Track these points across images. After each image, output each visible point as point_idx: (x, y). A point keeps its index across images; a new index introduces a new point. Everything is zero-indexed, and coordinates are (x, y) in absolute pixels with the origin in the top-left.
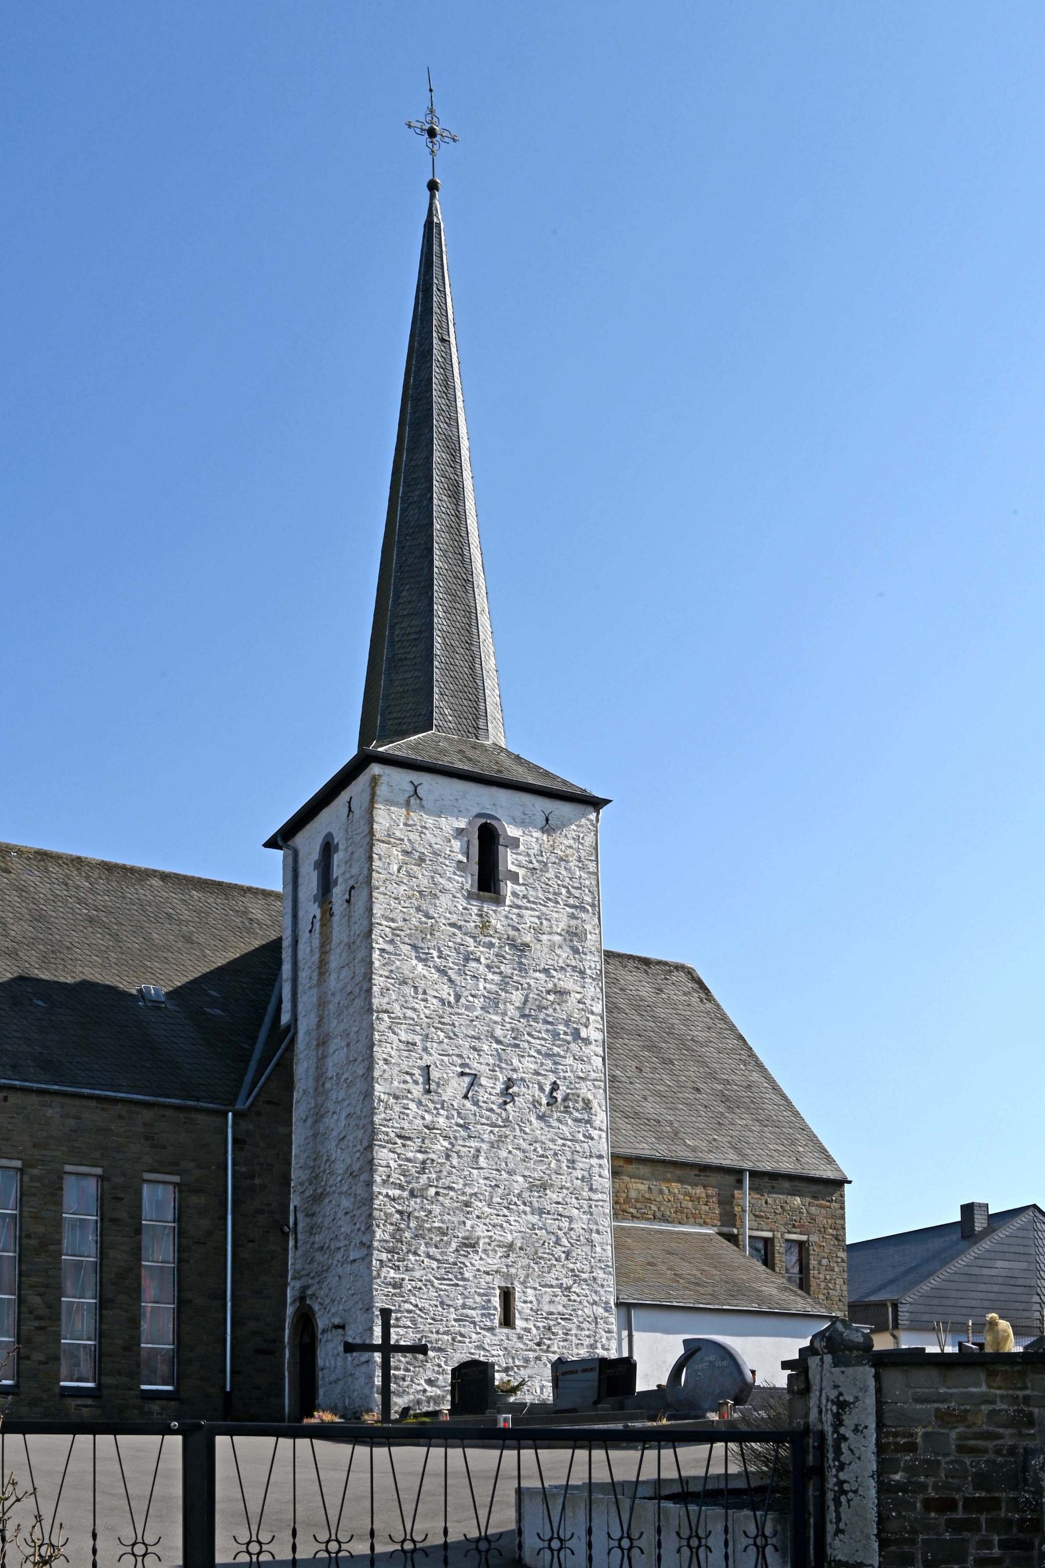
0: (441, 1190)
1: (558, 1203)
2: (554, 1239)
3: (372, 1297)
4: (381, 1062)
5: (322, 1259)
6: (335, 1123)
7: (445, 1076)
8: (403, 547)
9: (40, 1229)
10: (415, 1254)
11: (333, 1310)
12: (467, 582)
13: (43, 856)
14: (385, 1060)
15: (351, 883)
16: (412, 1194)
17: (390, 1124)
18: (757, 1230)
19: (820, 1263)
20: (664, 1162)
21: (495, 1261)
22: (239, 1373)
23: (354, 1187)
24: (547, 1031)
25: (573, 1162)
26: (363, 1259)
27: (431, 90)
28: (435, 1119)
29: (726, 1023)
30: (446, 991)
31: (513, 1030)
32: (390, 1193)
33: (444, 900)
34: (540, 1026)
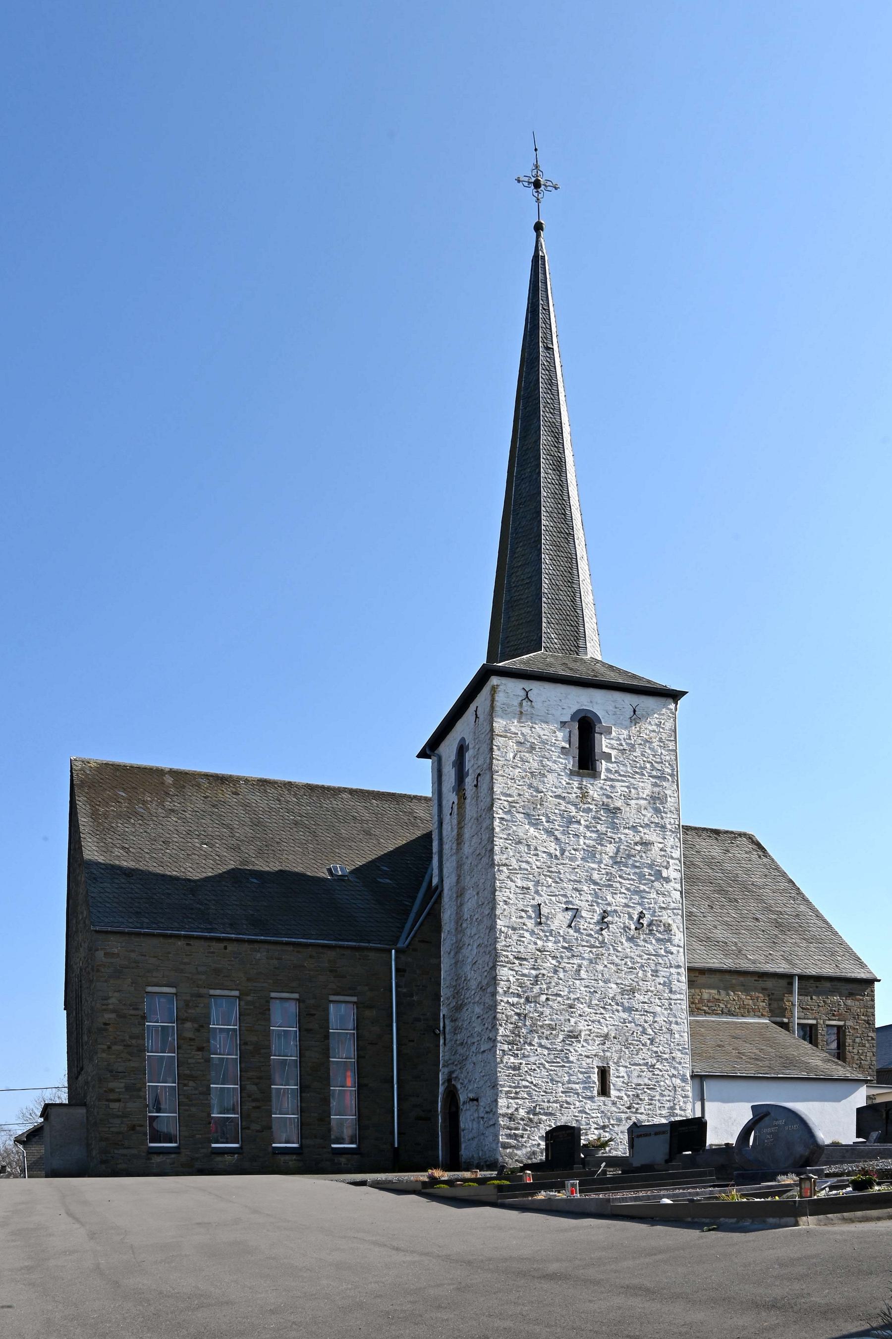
1: (645, 1003)
2: (641, 1029)
4: (501, 903)
5: (462, 1052)
6: (470, 953)
9: (254, 1039)
10: (530, 1044)
12: (569, 536)
13: (264, 782)
14: (505, 901)
15: (478, 771)
16: (528, 1000)
18: (804, 1019)
19: (854, 1041)
21: (594, 1048)
24: (635, 873)
25: (657, 971)
28: (545, 944)
30: (553, 847)
32: (510, 1000)
33: (551, 778)
34: (628, 870)
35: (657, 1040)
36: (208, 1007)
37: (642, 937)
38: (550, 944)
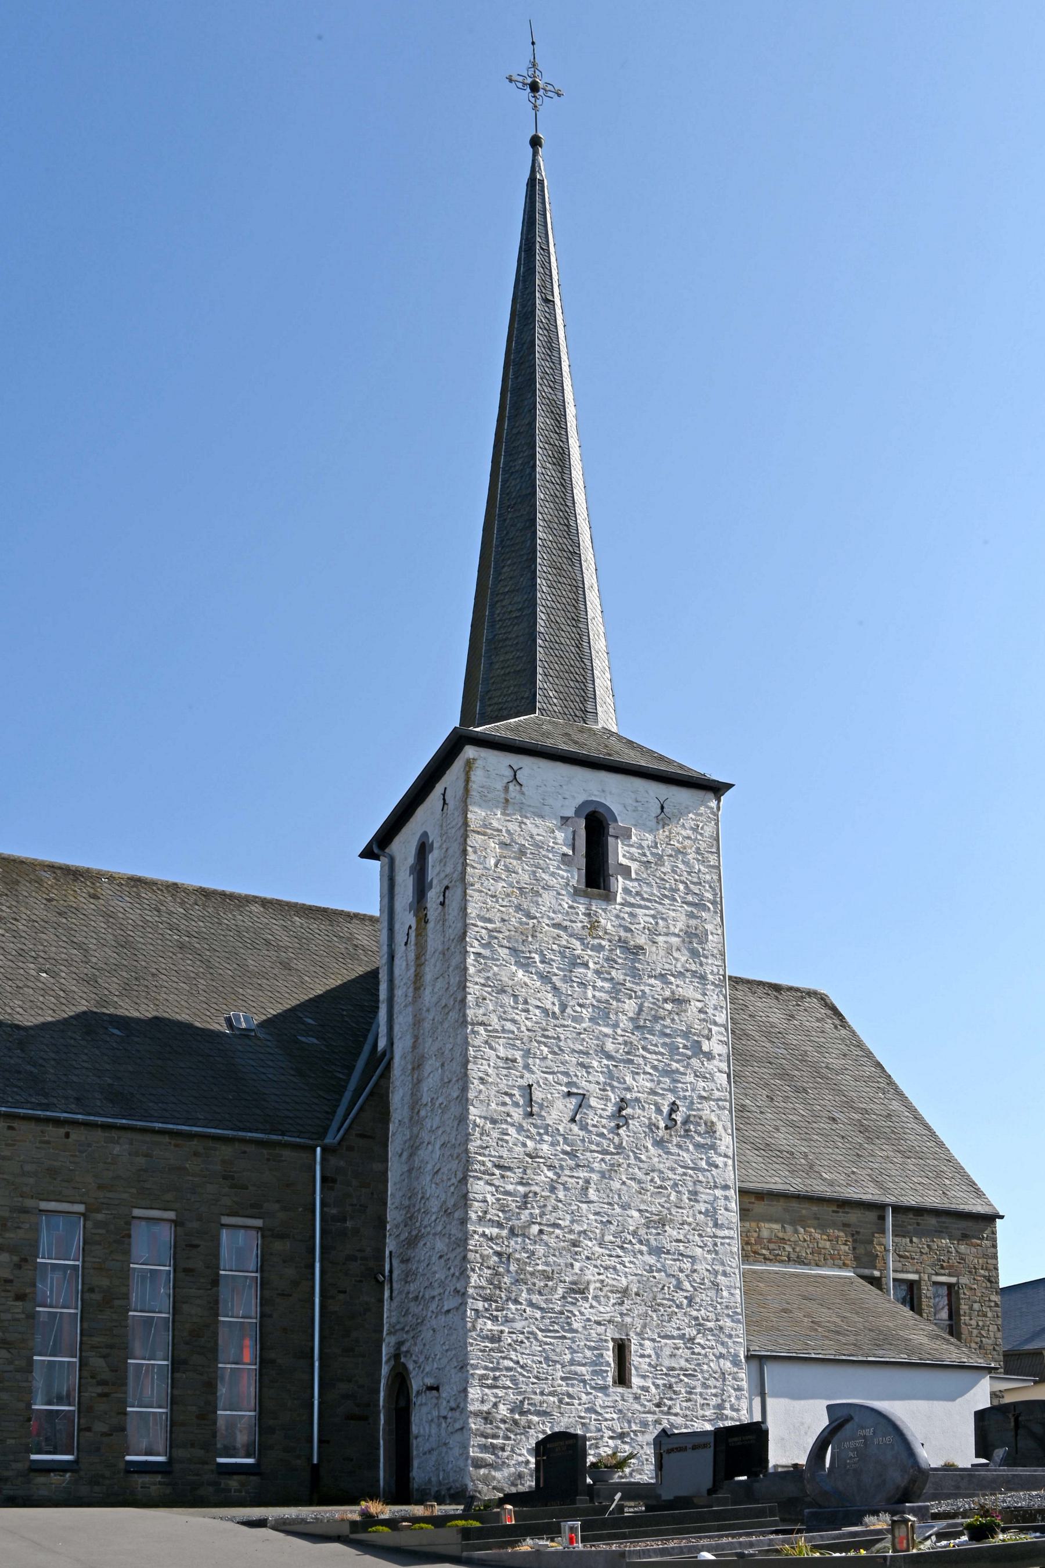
0: (545, 1228)
3: (466, 1354)
4: (476, 1082)
6: (431, 1155)
7: (549, 1096)
8: (505, 520)
9: (105, 1282)
10: (516, 1302)
11: (427, 1369)
12: (574, 555)
14: (481, 1079)
15: (446, 883)
16: (512, 1232)
17: (487, 1152)
18: (902, 1271)
19: (971, 1308)
20: (798, 1197)
21: (607, 1310)
22: (328, 1442)
23: (448, 1227)
25: (696, 1193)
26: (457, 1309)
27: (533, 43)
28: (538, 1146)
29: (862, 1050)
30: (549, 1000)
31: (626, 1043)
32: (487, 1231)
33: (547, 898)
35: (698, 1300)
36: (36, 1229)
37: (675, 1140)
38: (545, 1147)
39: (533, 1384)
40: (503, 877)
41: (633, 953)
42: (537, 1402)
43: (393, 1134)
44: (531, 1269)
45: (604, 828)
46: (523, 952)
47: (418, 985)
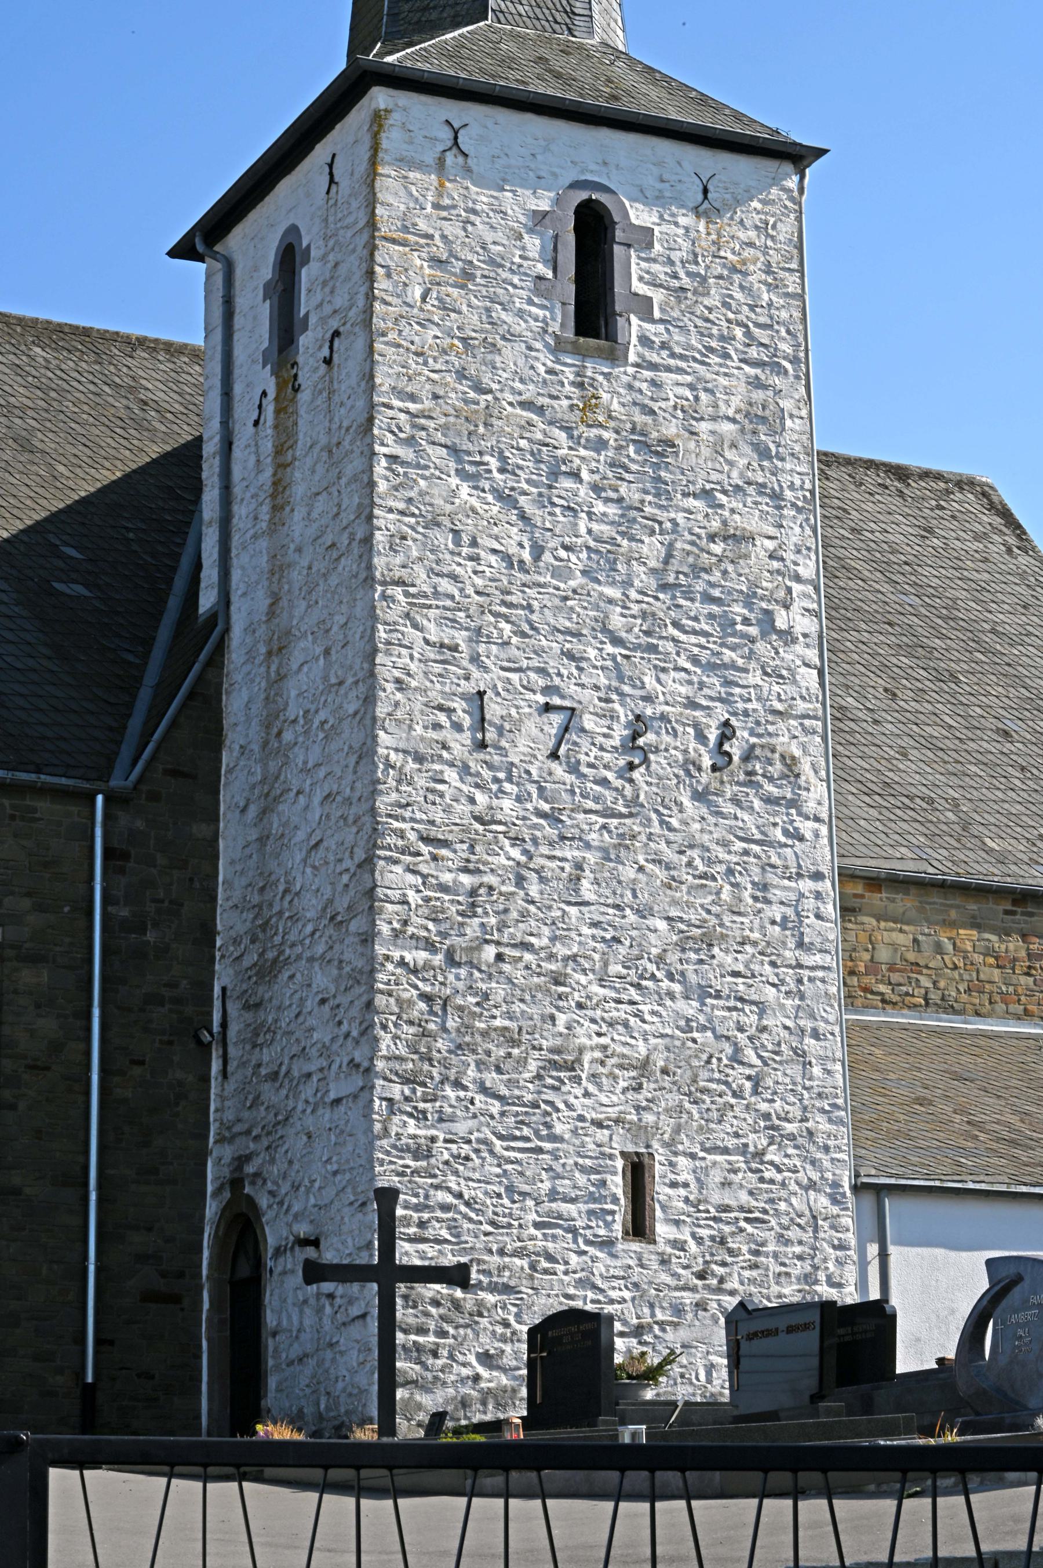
0: (507, 951)
1: (736, 974)
4: (390, 687)
5: (275, 1099)
6: (302, 815)
7: (513, 712)
10: (458, 1084)
14: (398, 681)
15: (334, 324)
16: (451, 960)
17: (408, 814)
21: (612, 1100)
22: (111, 1343)
23: (337, 947)
25: (765, 887)
26: (355, 1097)
28: (495, 802)
30: (514, 539)
32: (409, 958)
33: (511, 355)
35: (769, 1082)
37: (729, 791)
38: (507, 804)
39: (486, 1234)
40: (436, 319)
41: (657, 453)
42: (493, 1267)
43: (230, 771)
44: (483, 1025)
45: (606, 229)
46: (469, 453)
47: (279, 501)
